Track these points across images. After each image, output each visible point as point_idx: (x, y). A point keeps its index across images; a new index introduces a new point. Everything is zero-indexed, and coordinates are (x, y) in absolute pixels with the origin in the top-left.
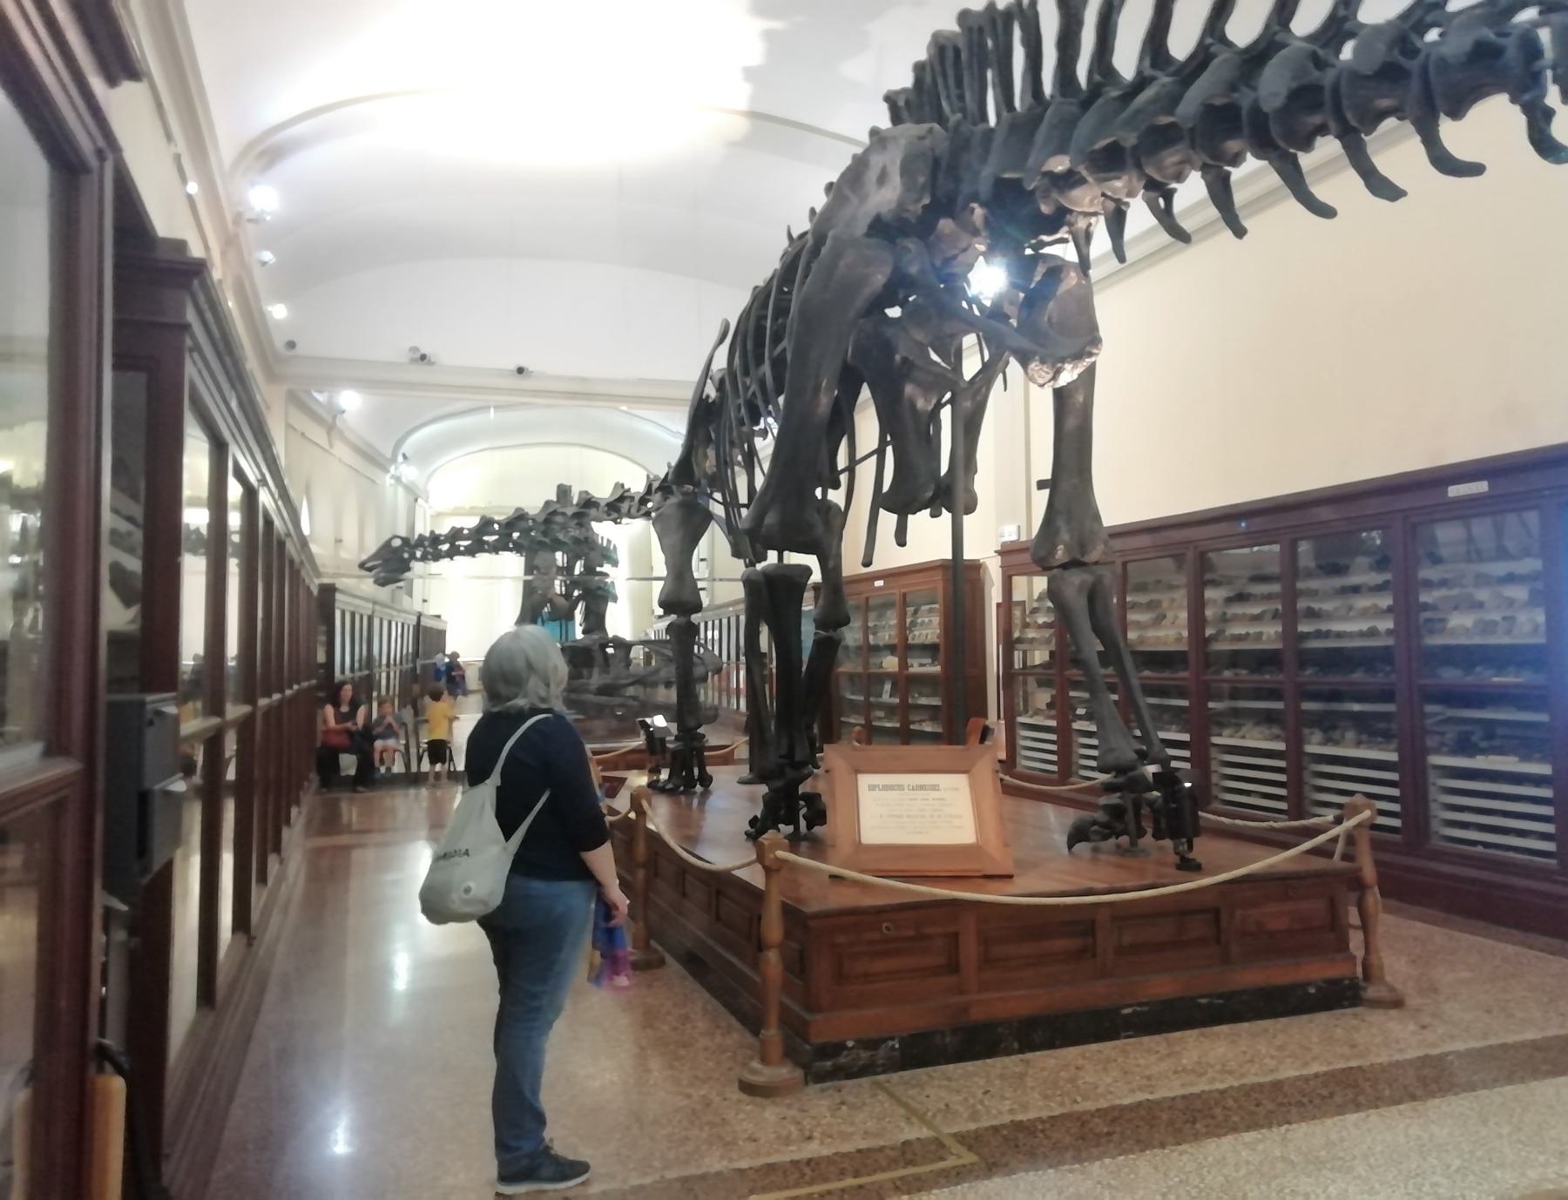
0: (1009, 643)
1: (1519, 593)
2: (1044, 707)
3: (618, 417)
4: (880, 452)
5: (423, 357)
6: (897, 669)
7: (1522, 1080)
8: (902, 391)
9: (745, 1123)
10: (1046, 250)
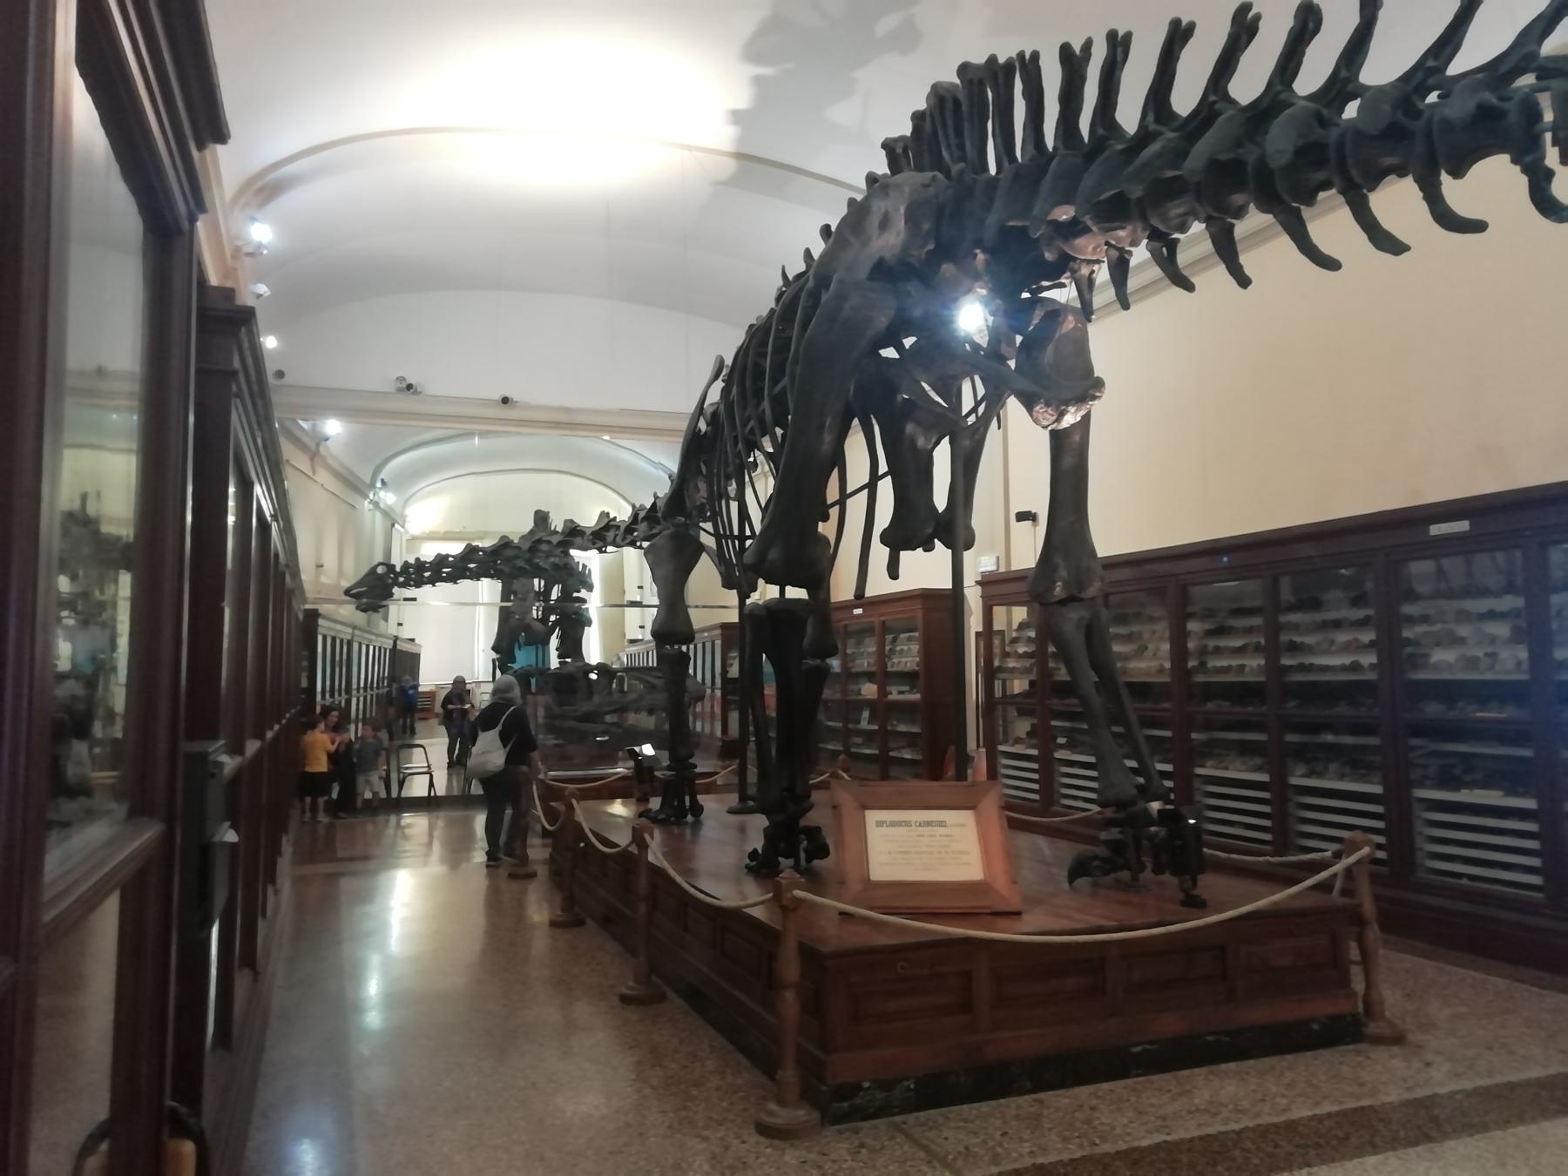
0: (990, 673)
1: (1502, 630)
2: (1024, 736)
3: (602, 445)
4: (871, 487)
5: (410, 387)
6: (876, 697)
7: (1533, 1120)
8: (903, 430)
9: (766, 1167)
10: (1045, 294)
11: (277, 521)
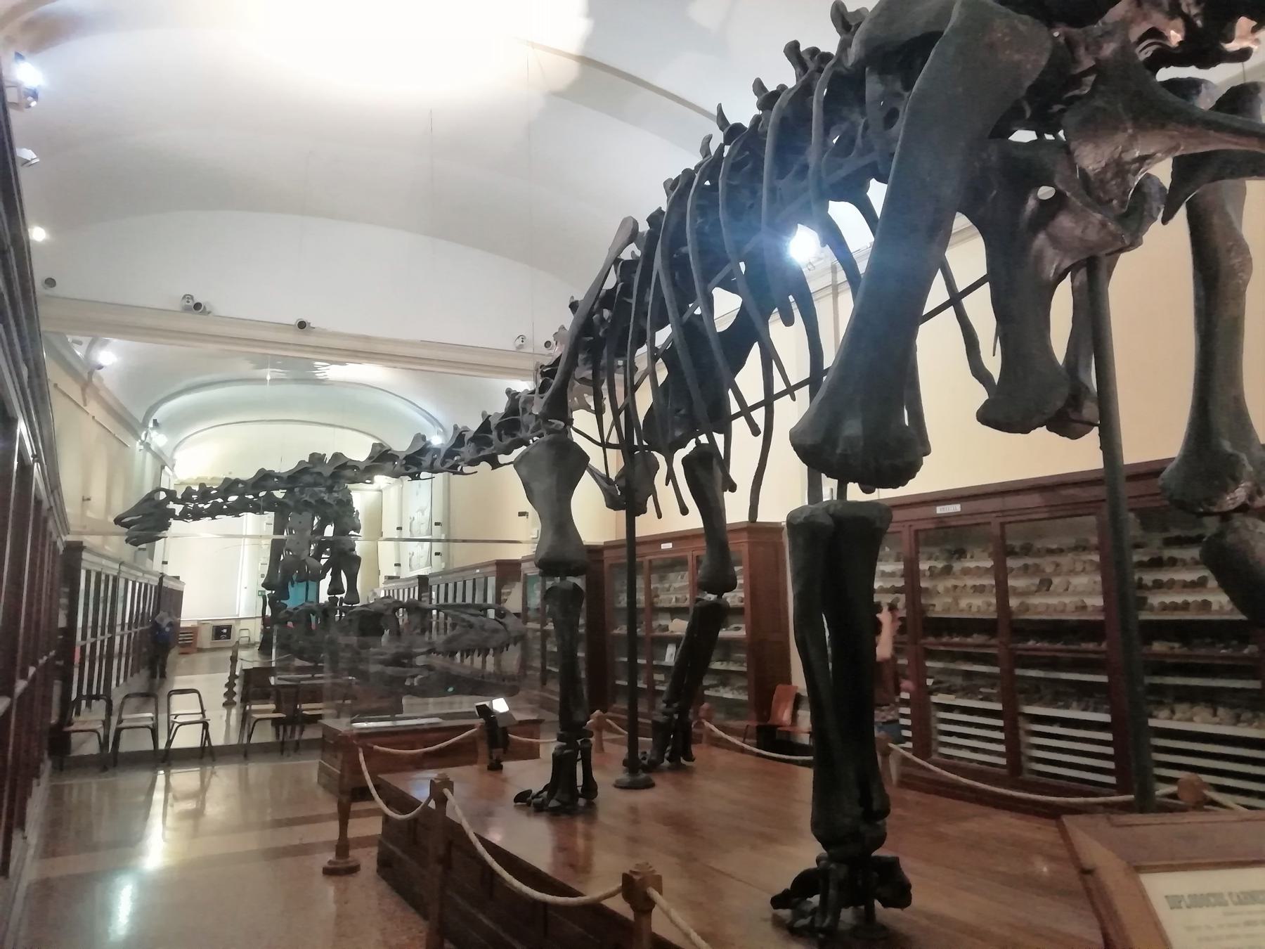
5: (197, 306)
11: (39, 461)
